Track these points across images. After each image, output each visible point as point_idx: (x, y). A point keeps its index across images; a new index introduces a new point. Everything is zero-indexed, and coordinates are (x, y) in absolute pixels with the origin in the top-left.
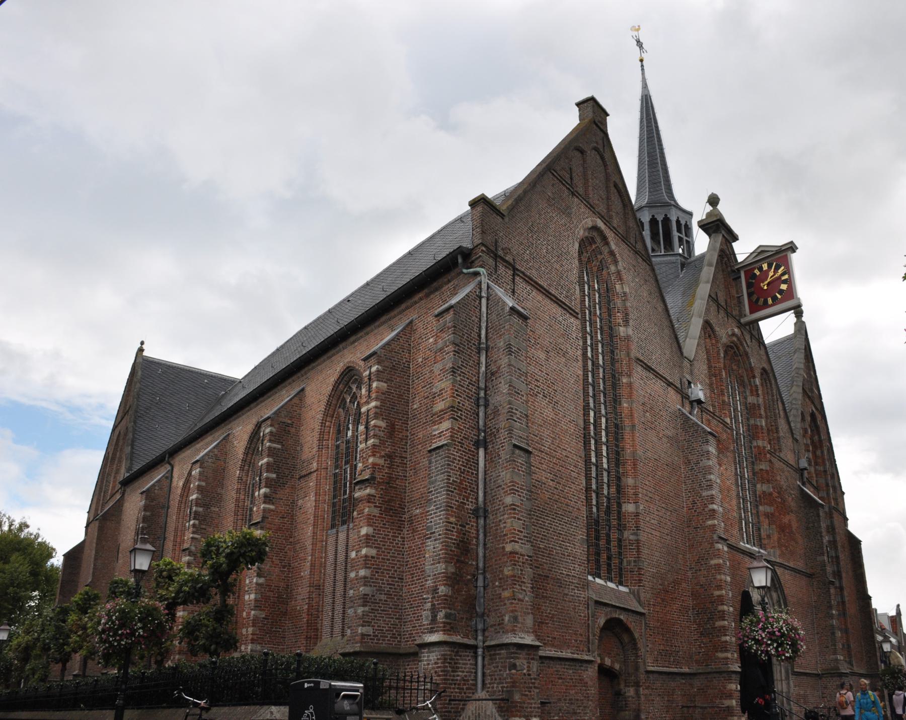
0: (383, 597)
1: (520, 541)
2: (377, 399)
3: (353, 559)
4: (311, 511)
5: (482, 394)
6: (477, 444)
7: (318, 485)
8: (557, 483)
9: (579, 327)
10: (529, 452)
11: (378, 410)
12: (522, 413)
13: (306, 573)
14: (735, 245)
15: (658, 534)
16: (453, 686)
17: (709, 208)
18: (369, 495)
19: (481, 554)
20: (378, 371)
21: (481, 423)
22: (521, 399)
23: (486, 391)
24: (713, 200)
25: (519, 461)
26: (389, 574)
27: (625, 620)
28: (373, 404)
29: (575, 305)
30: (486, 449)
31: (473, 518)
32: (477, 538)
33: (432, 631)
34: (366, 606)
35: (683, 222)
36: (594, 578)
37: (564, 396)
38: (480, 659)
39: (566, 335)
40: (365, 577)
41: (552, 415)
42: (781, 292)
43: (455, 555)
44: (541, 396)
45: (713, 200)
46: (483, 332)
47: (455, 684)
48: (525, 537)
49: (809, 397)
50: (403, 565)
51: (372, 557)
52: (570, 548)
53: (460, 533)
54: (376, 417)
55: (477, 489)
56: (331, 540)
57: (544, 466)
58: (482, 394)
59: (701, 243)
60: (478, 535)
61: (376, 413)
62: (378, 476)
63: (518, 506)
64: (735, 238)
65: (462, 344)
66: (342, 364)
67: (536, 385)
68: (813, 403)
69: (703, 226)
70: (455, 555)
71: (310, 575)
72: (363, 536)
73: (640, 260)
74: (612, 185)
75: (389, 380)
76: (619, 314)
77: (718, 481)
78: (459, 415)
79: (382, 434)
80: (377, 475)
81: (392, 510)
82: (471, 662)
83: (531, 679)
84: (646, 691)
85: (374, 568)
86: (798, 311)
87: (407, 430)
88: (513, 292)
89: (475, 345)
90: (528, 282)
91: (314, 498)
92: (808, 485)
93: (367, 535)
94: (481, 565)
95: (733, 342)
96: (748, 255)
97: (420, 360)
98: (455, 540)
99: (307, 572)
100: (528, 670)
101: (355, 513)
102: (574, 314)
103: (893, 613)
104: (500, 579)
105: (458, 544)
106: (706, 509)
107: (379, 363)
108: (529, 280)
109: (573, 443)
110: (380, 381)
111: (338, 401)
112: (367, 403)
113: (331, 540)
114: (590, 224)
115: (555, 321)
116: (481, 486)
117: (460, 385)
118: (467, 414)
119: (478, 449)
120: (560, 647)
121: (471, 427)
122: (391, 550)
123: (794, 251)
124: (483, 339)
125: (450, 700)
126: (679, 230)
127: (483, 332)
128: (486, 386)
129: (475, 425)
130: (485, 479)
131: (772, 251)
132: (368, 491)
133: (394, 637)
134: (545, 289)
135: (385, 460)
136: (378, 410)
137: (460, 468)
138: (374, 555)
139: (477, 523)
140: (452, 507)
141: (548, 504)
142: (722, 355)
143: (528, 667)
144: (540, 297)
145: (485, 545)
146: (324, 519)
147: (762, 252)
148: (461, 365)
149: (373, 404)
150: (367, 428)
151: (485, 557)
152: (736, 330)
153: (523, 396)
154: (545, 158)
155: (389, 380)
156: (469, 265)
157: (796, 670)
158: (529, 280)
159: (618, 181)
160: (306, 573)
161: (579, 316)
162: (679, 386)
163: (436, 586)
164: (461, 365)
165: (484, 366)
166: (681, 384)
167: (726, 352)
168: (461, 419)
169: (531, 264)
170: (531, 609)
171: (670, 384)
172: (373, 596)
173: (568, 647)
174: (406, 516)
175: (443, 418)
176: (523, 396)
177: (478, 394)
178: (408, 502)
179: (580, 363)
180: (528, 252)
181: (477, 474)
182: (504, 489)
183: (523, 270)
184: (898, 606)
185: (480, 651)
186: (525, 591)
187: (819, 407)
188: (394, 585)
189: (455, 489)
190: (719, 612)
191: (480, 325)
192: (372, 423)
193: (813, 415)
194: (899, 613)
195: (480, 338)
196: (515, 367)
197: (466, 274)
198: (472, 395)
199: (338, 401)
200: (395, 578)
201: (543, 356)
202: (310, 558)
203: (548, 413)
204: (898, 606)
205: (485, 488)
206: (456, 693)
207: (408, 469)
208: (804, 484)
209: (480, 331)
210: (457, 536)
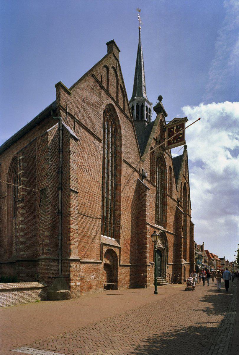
0: (29, 242)
1: (73, 224)
2: (23, 170)
3: (18, 229)
4: (6, 210)
5: (60, 170)
6: (59, 189)
7: (8, 201)
8: (91, 203)
9: (102, 146)
10: (77, 193)
11: (24, 174)
12: (75, 178)
13: (6, 232)
14: (166, 118)
15: (127, 222)
16: (50, 273)
17: (158, 102)
18: (22, 206)
19: (60, 228)
20: (23, 158)
21: (60, 180)
22: (75, 172)
23: (62, 169)
24: (160, 98)
25: (74, 196)
26: (31, 234)
27: (114, 250)
28: (22, 171)
29: (101, 137)
30: (62, 191)
31: (57, 216)
32: (59, 223)
33: (43, 255)
34: (23, 245)
35: (148, 108)
36: (104, 236)
37: (95, 172)
38: (60, 264)
39: (96, 149)
40: (22, 235)
41: (89, 179)
42: (179, 138)
43: (50, 229)
44: (85, 172)
45: (160, 98)
46: (61, 145)
47: (51, 272)
48: (75, 223)
49: (184, 177)
50: (36, 231)
51: (24, 228)
52: (95, 226)
53: (52, 221)
54: (23, 176)
55: (59, 205)
56: (14, 221)
57: (86, 198)
58: (60, 170)
59: (154, 116)
60: (59, 221)
61: (23, 175)
62: (25, 199)
63: (73, 212)
64: (166, 116)
65: (52, 149)
66: (13, 155)
67: (83, 167)
68: (186, 179)
69: (156, 109)
70: (50, 229)
71: (8, 233)
72: (20, 221)
73: (128, 121)
74: (119, 86)
75: (27, 162)
76: (118, 142)
77: (149, 205)
78: (51, 177)
79: (26, 183)
80: (24, 198)
81: (31, 211)
82: (57, 265)
83: (77, 270)
84: (120, 271)
85: (25, 232)
86: (186, 147)
87: (36, 182)
88: (74, 129)
89: (57, 149)
90: (81, 125)
91: (7, 206)
92: (180, 207)
93: (22, 220)
94: (60, 232)
95: (160, 156)
96: (169, 122)
97: (40, 155)
98: (50, 223)
99: (7, 232)
100: (76, 268)
101: (17, 212)
102: (100, 140)
103: (202, 245)
104: (67, 237)
105: (51, 225)
106: (144, 214)
107: (23, 155)
108: (81, 125)
109: (97, 190)
110: (24, 162)
111: (13, 170)
112: (20, 171)
113: (14, 221)
114: (109, 103)
115: (92, 143)
116: (60, 204)
117: (51, 165)
118: (55, 177)
119: (59, 190)
120: (90, 258)
121: (56, 182)
122: (31, 226)
123: (186, 122)
124: (61, 148)
125: (49, 277)
126: (147, 111)
127: (61, 145)
128: (62, 167)
129: (58, 181)
130: (62, 202)
131: (178, 121)
132: (21, 205)
133: (34, 255)
134: (88, 129)
135: (27, 193)
136: (24, 174)
137: (51, 198)
138: (25, 227)
139: (59, 217)
140: (49, 212)
141: (87, 211)
142: (156, 160)
143: (76, 266)
144: (86, 132)
145: (62, 225)
146: (11, 213)
147: (175, 121)
148: (52, 157)
149: (22, 171)
150: (20, 180)
151: (62, 230)
152: (162, 152)
153: (76, 171)
154: (133, 92)
155: (27, 162)
156: (56, 115)
157: (168, 263)
158: (81, 125)
159: (122, 85)
160: (6, 232)
161: (102, 141)
162: (138, 171)
163: (44, 239)
164: (52, 157)
165: (61, 158)
166: (139, 170)
167: (157, 160)
168: (52, 179)
169: (82, 117)
170: (77, 248)
171: (135, 170)
172: (25, 241)
173: (93, 258)
174: (37, 213)
175: (45, 178)
176: (76, 171)
177: (59, 170)
178: (37, 209)
179: (102, 160)
180: (81, 112)
181: (59, 200)
182: (67, 205)
183: (79, 120)
184: (204, 243)
185: (60, 261)
186: (75, 241)
187: (187, 181)
188: (33, 238)
189: (50, 205)
190: (145, 247)
191: (60, 141)
192: (22, 179)
193: (185, 184)
194: (203, 244)
195: (60, 147)
196: (72, 159)
197: (55, 119)
198: (56, 170)
199: (13, 170)
200: (33, 235)
201: (86, 156)
202: (7, 227)
203: (88, 178)
204: (204, 243)
205: (62, 205)
206: (51, 275)
207: (37, 197)
208: (178, 206)
209: (60, 144)
210: (51, 222)
